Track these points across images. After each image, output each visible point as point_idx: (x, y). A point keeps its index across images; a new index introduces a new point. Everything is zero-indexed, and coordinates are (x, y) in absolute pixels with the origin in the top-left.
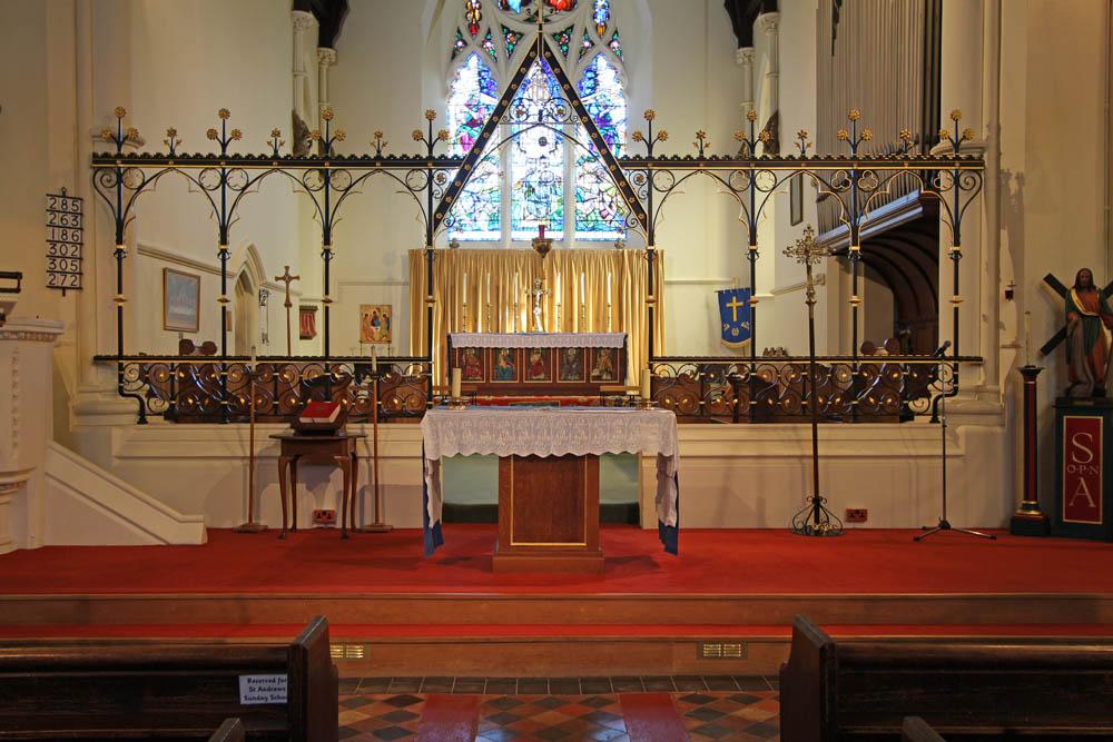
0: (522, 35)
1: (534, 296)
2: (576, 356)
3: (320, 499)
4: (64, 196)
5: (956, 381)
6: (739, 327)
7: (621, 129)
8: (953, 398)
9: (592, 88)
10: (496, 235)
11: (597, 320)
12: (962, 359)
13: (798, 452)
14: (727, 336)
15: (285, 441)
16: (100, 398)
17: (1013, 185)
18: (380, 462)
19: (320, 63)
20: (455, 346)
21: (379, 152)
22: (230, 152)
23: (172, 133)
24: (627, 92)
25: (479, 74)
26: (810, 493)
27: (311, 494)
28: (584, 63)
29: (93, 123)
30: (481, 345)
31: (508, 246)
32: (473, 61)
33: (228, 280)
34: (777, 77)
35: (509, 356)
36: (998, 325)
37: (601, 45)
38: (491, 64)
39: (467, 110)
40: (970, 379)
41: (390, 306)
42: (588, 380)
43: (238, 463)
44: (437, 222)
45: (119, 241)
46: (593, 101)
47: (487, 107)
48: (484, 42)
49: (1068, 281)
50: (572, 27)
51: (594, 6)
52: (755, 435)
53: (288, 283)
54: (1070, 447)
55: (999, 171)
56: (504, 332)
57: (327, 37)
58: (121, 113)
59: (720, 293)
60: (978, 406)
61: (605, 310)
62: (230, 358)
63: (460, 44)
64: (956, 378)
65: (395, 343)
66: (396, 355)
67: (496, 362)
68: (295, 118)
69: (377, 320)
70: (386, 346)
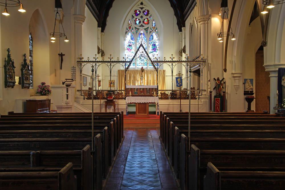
1: (141, 78)
7: (158, 47)
10: (134, 67)
11: (153, 83)
14: (177, 86)
16: (78, 96)
17: (210, 65)
19: (101, 35)
22: (97, 61)
23: (88, 58)
24: (159, 40)
29: (77, 56)
30: (76, 74)
32: (130, 34)
36: (208, 85)
37: (154, 31)
41: (114, 80)
43: (98, 105)
44: (127, 70)
45: (81, 73)
50: (148, 27)
51: (153, 23)
52: (173, 101)
54: (216, 103)
55: (208, 63)
57: (102, 31)
58: (81, 55)
59: (176, 78)
60: (205, 97)
61: (154, 81)
62: (97, 90)
63: (127, 31)
65: (115, 87)
66: (115, 90)
67: (134, 91)
68: (98, 47)
69: (111, 83)
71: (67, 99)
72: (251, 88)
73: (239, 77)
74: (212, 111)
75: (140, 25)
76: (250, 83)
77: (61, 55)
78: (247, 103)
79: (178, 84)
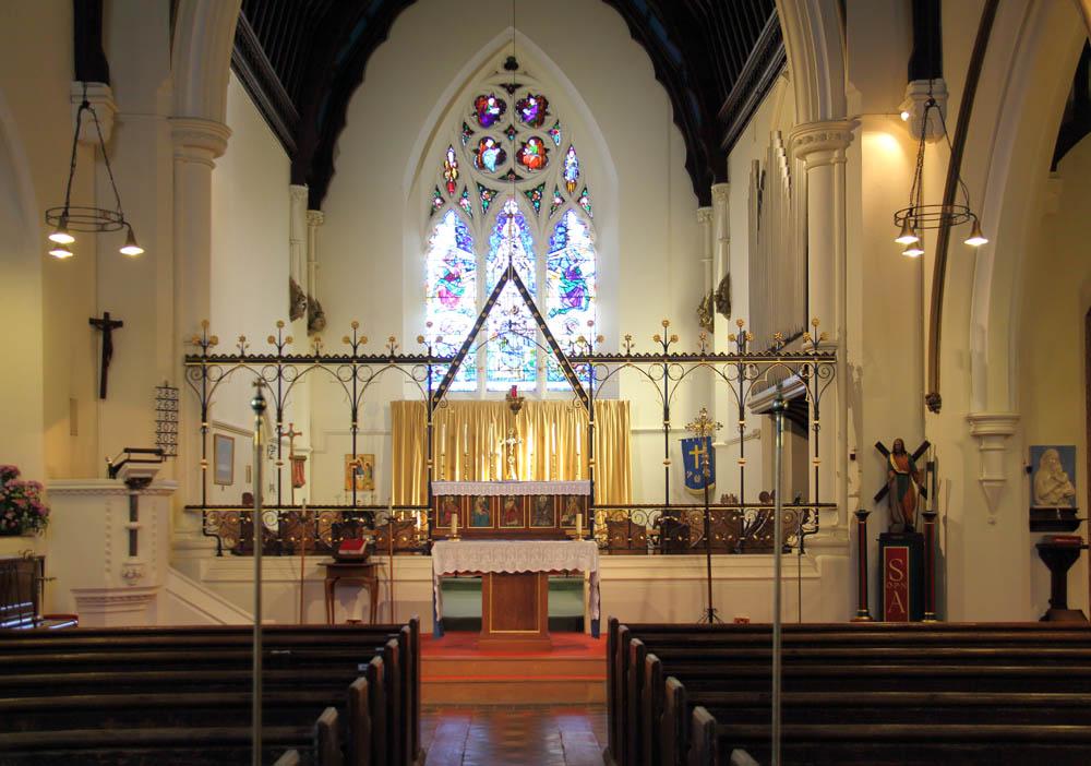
0: (496, 192)
1: (508, 445)
2: (547, 503)
3: (351, 611)
4: (166, 388)
5: (817, 522)
6: (701, 474)
7: (590, 282)
8: (816, 535)
9: (563, 243)
10: (473, 386)
11: (568, 468)
12: (822, 505)
13: (699, 576)
15: (330, 567)
16: (189, 537)
17: (855, 375)
18: (395, 584)
19: (309, 225)
20: (435, 494)
21: (392, 352)
22: (284, 354)
24: (596, 247)
25: (457, 231)
26: (707, 606)
27: (344, 609)
28: (555, 219)
31: (484, 397)
33: (282, 448)
34: (728, 242)
35: (485, 503)
36: (847, 480)
37: (570, 201)
38: (469, 223)
39: (445, 264)
40: (826, 520)
42: (558, 525)
43: (291, 585)
44: (435, 404)
45: (204, 420)
46: (563, 255)
47: (464, 262)
48: (460, 200)
49: (890, 448)
50: (543, 185)
51: (564, 164)
53: (292, 438)
54: (889, 569)
56: (480, 481)
57: (315, 202)
59: (683, 441)
63: (438, 201)
64: (817, 519)
65: (378, 492)
67: (473, 508)
69: (358, 469)
70: (369, 494)
71: (133, 552)
72: (1065, 496)
73: (1007, 436)
74: (867, 614)
75: (503, 170)
76: (1059, 467)
77: (106, 327)
78: (1045, 575)
79: (696, 472)
